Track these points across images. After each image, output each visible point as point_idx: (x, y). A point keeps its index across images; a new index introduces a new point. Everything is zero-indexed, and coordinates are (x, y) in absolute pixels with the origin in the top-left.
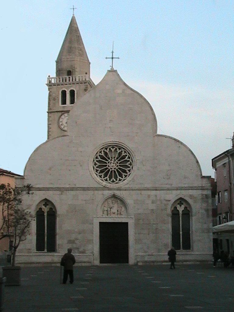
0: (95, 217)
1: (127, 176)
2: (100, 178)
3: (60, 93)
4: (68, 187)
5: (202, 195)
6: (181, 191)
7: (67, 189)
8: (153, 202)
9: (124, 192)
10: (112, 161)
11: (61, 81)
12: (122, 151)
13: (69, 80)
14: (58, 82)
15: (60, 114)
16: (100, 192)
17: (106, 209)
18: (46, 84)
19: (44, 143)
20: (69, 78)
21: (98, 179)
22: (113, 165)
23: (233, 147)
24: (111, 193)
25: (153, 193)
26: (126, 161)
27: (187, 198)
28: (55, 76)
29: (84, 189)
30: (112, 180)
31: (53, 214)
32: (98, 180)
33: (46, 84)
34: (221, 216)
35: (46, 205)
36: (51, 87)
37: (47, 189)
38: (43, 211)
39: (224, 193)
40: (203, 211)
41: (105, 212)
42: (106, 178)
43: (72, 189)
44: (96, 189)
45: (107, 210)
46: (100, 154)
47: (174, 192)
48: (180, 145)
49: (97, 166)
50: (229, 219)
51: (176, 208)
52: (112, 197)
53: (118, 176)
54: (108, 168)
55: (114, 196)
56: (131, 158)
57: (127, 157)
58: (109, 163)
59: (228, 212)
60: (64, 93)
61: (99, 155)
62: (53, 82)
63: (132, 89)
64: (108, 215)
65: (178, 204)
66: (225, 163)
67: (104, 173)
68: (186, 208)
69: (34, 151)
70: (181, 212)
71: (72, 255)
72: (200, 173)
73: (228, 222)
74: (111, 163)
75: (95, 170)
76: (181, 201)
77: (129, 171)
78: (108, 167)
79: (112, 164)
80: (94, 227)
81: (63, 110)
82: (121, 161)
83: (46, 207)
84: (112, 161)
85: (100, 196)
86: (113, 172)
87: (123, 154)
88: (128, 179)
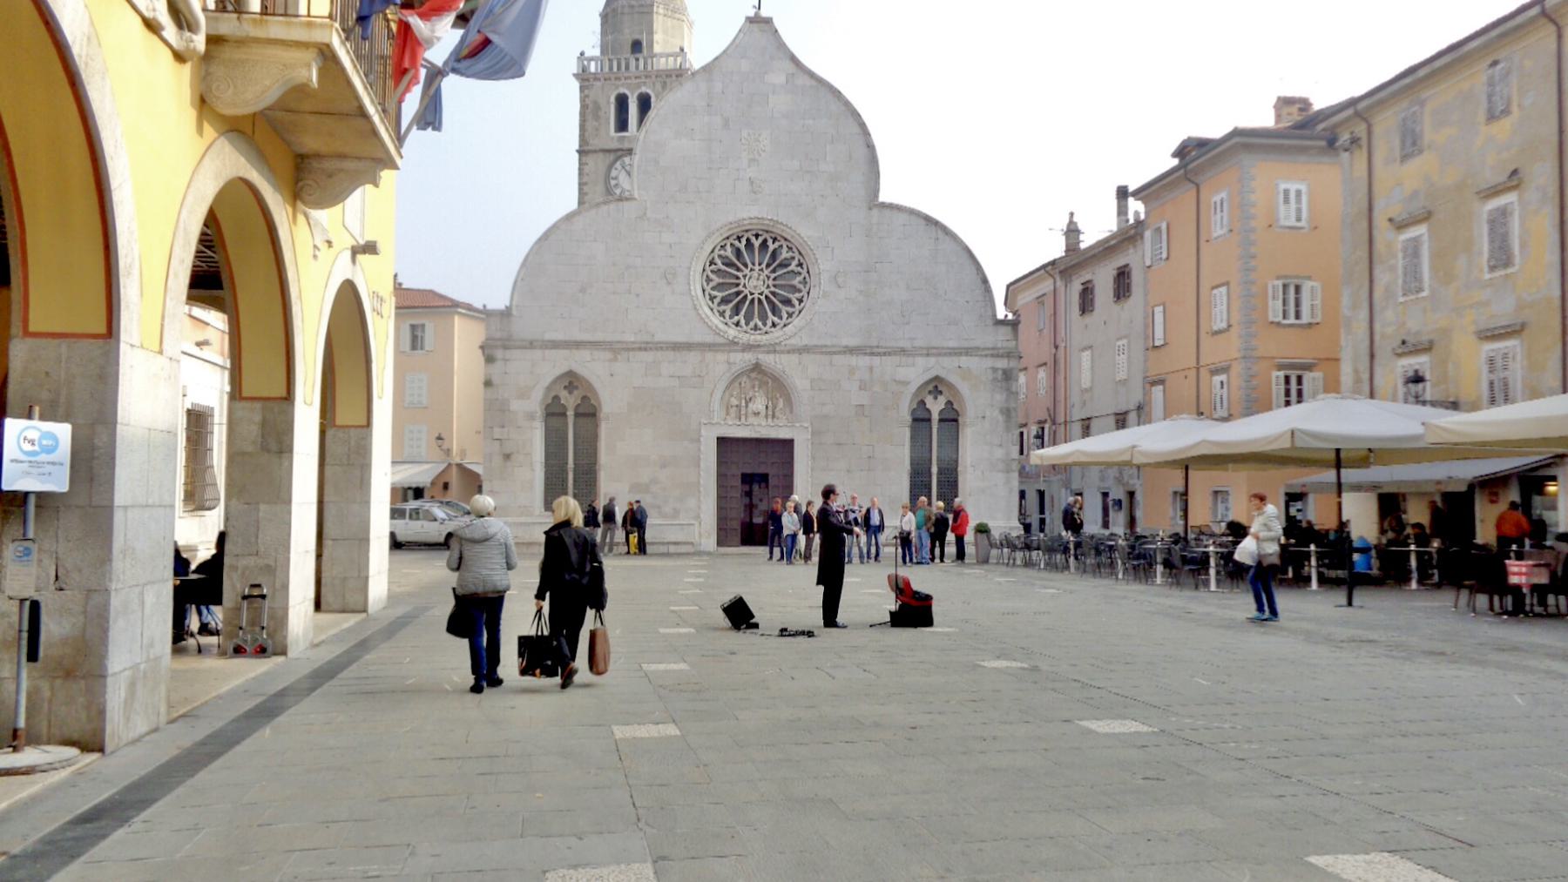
0: (705, 422)
1: (794, 316)
2: (722, 319)
3: (613, 99)
4: (632, 339)
5: (995, 370)
6: (940, 359)
7: (630, 346)
8: (863, 387)
9: (785, 357)
10: (755, 274)
11: (615, 69)
12: (781, 246)
13: (637, 67)
14: (606, 69)
15: (612, 157)
16: (721, 357)
17: (734, 402)
18: (574, 75)
19: (569, 217)
20: (637, 60)
21: (716, 321)
22: (755, 282)
23: (1066, 251)
24: (749, 358)
25: (863, 361)
26: (791, 274)
27: (953, 379)
28: (597, 52)
29: (676, 347)
30: (752, 324)
31: (589, 413)
32: (714, 322)
33: (574, 75)
34: (1025, 431)
35: (570, 387)
36: (587, 83)
37: (578, 345)
38: (563, 404)
39: (1038, 372)
40: (996, 413)
41: (733, 411)
42: (736, 318)
43: (645, 347)
44: (711, 347)
45: (737, 406)
46: (722, 252)
47: (920, 361)
48: (941, 234)
49: (712, 284)
50: (1046, 438)
51: (922, 403)
52: (752, 370)
53: (770, 314)
54: (742, 292)
55: (757, 367)
56: (805, 266)
57: (795, 263)
58: (745, 276)
59: (1045, 421)
60: (622, 102)
61: (720, 256)
62: (593, 69)
63: (812, 75)
64: (740, 419)
65: (930, 392)
66: (1044, 295)
67: (731, 305)
68: (949, 403)
69: (540, 240)
70: (935, 417)
71: (1379, 569)
72: (990, 313)
73: (1043, 447)
74: (750, 278)
75: (708, 297)
76: (936, 386)
77: (801, 301)
78: (743, 289)
79: (754, 282)
80: (702, 448)
81: (620, 147)
82: (777, 274)
83: (570, 393)
84: (755, 274)
85: (721, 367)
86: (777, 282)
87: (785, 254)
88: (797, 322)
